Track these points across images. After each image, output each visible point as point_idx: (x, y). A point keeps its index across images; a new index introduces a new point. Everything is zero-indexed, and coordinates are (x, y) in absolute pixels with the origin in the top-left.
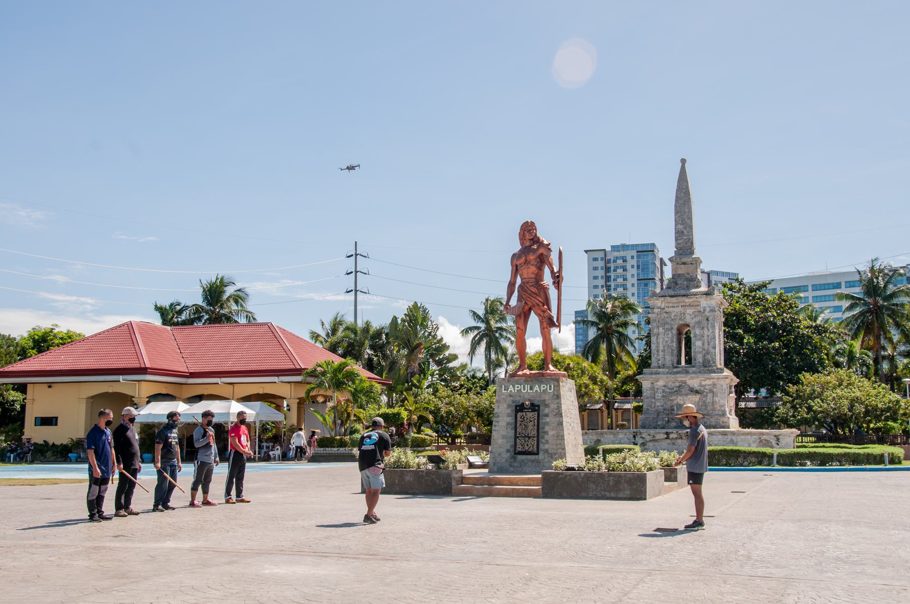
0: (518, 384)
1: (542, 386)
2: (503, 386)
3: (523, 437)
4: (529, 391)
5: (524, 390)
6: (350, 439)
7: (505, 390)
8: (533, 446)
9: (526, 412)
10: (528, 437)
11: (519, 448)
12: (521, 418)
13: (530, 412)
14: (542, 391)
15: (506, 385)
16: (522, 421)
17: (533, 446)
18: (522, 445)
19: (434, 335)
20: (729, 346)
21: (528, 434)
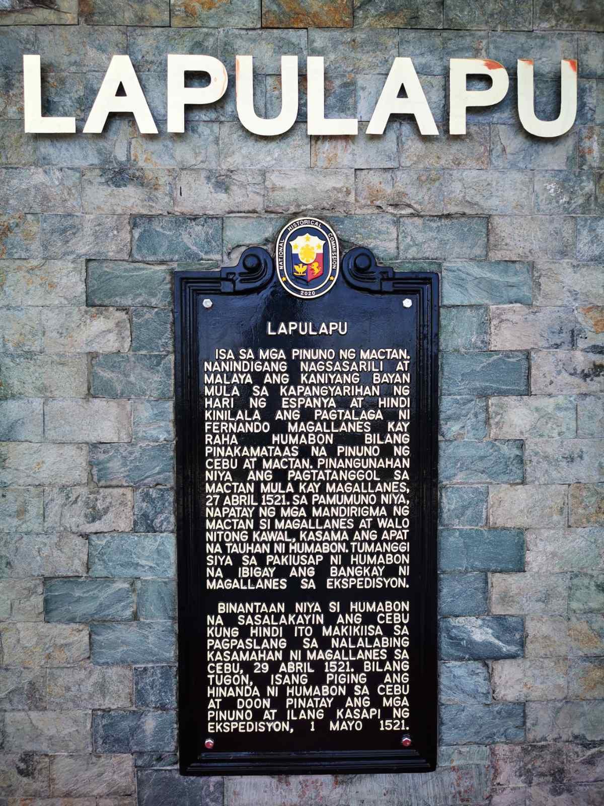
0: (198, 48)
1: (291, 323)
2: (32, 65)
3: (268, 596)
4: (318, 124)
5: (265, 110)
6: (247, 468)
7: (47, 109)
8: (374, 679)
9: (297, 341)
10: (322, 595)
11: (229, 704)
12: (241, 403)
13: (336, 342)
14: (458, 125)
15: (62, 57)
16: (262, 440)
17: (374, 679)
18: (261, 681)
19: (376, 627)
20: (255, 450)
21: (322, 570)
